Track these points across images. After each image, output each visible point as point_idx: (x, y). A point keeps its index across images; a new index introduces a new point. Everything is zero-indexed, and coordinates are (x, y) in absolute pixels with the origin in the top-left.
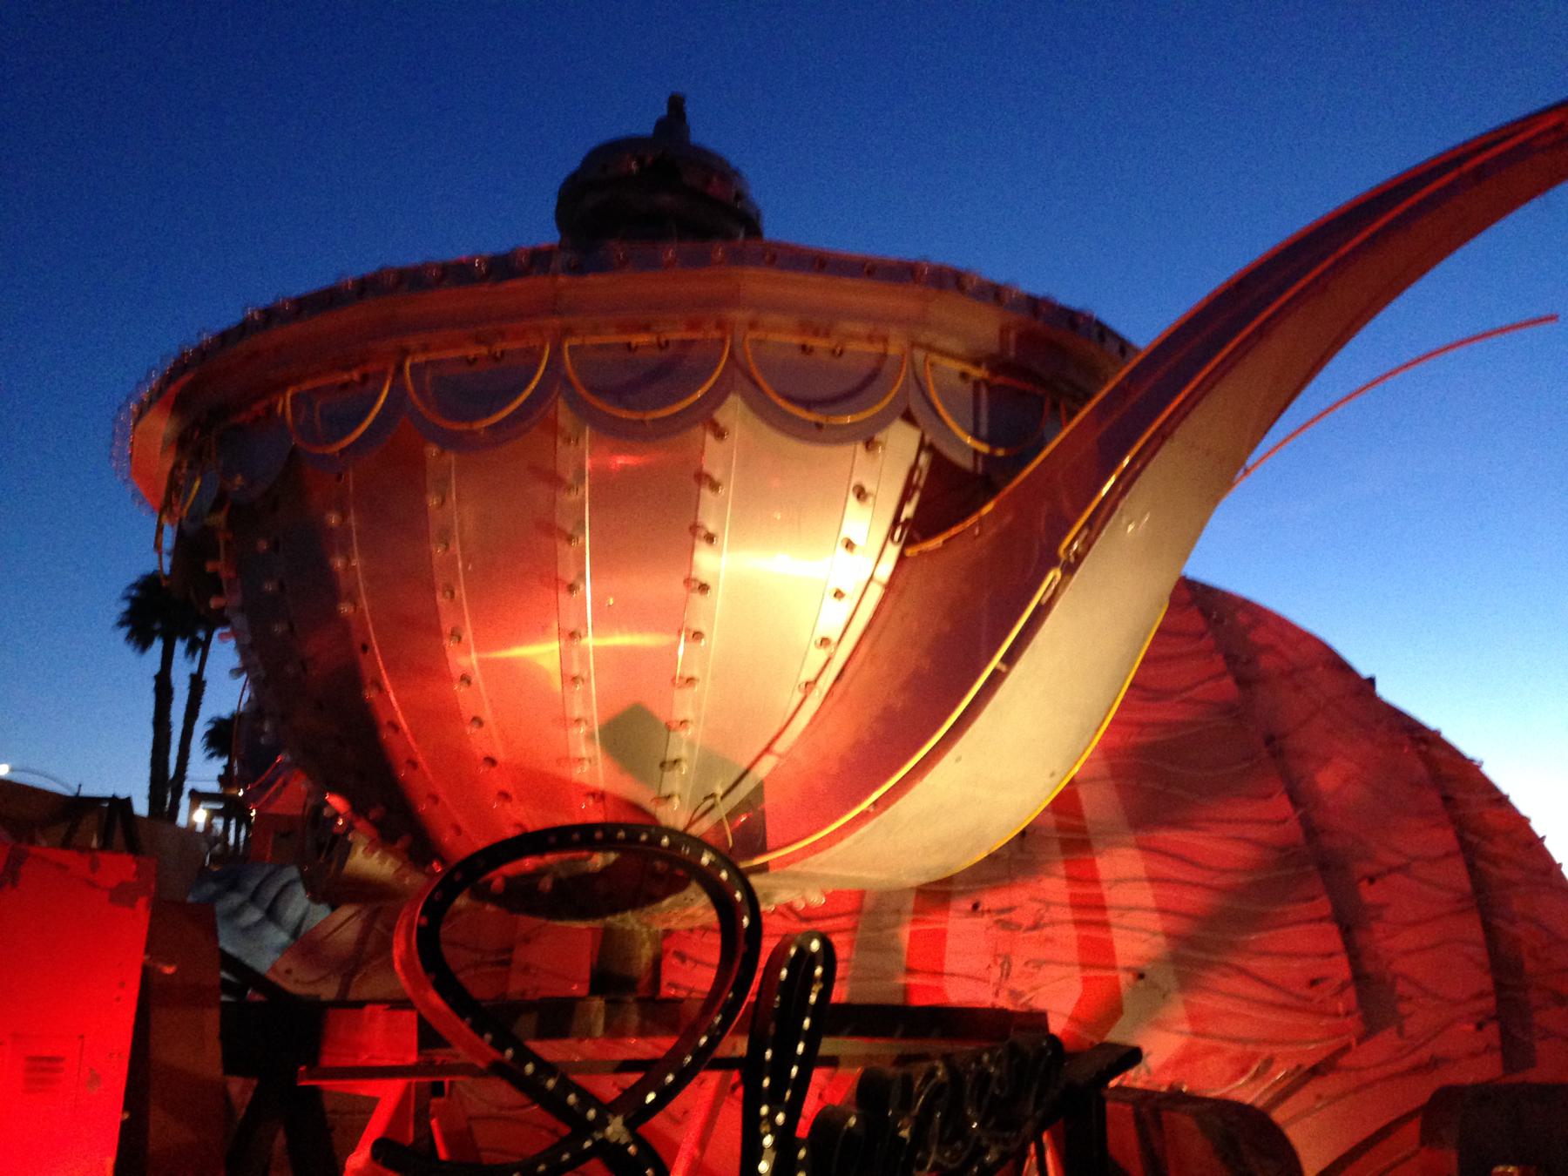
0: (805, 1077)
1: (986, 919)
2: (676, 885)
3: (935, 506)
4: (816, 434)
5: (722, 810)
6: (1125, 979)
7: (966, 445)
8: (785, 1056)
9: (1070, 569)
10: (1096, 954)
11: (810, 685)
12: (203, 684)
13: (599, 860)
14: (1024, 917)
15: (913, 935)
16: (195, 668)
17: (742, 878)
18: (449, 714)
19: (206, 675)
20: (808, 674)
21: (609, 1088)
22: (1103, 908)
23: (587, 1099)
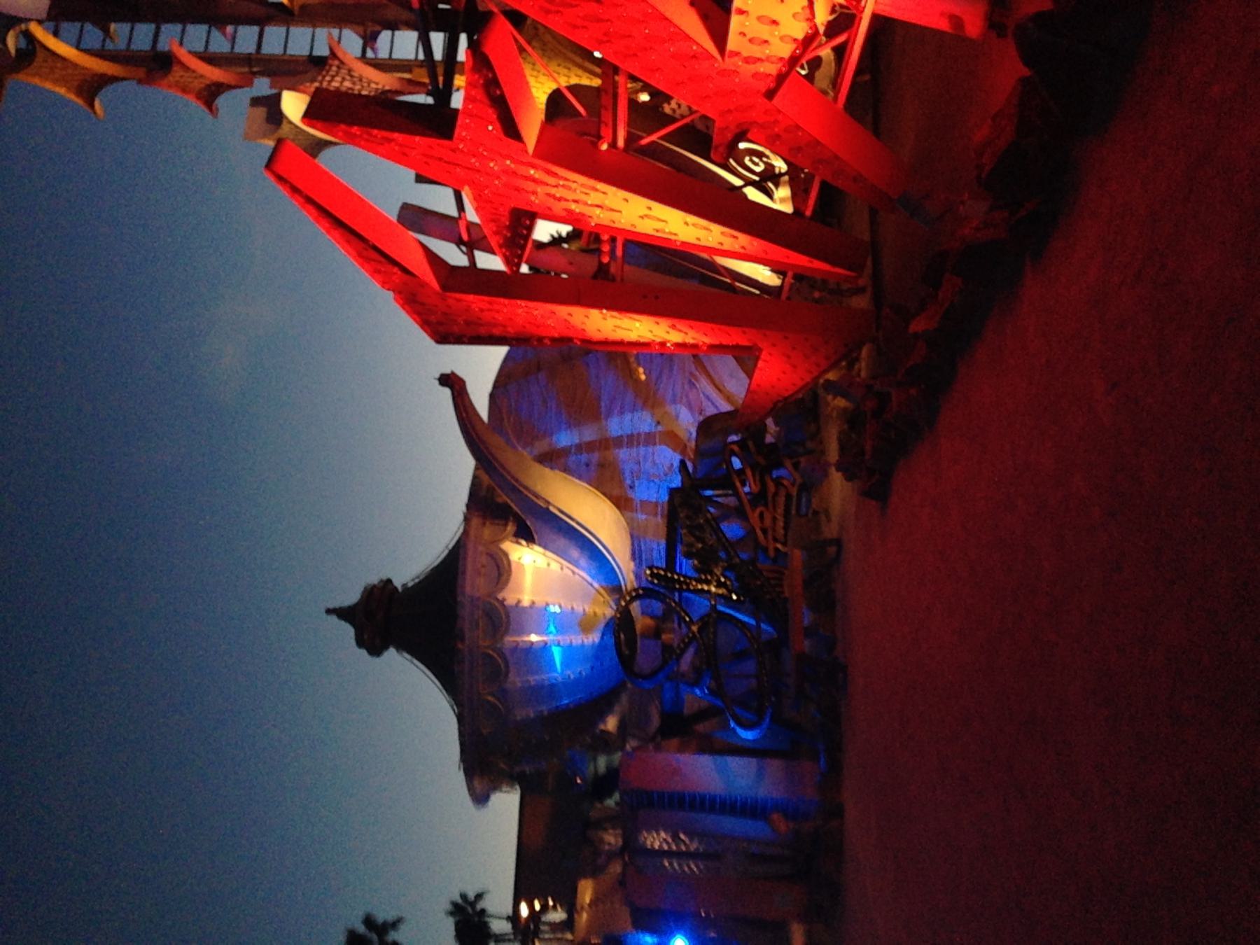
0: (684, 576)
1: (637, 483)
2: (629, 612)
3: (526, 535)
5: (608, 598)
6: (660, 428)
7: (511, 528)
8: (678, 581)
9: (548, 503)
10: (650, 439)
11: (574, 573)
14: (636, 468)
15: (642, 512)
17: (629, 593)
18: (577, 682)
20: (570, 573)
21: (684, 630)
22: (632, 435)
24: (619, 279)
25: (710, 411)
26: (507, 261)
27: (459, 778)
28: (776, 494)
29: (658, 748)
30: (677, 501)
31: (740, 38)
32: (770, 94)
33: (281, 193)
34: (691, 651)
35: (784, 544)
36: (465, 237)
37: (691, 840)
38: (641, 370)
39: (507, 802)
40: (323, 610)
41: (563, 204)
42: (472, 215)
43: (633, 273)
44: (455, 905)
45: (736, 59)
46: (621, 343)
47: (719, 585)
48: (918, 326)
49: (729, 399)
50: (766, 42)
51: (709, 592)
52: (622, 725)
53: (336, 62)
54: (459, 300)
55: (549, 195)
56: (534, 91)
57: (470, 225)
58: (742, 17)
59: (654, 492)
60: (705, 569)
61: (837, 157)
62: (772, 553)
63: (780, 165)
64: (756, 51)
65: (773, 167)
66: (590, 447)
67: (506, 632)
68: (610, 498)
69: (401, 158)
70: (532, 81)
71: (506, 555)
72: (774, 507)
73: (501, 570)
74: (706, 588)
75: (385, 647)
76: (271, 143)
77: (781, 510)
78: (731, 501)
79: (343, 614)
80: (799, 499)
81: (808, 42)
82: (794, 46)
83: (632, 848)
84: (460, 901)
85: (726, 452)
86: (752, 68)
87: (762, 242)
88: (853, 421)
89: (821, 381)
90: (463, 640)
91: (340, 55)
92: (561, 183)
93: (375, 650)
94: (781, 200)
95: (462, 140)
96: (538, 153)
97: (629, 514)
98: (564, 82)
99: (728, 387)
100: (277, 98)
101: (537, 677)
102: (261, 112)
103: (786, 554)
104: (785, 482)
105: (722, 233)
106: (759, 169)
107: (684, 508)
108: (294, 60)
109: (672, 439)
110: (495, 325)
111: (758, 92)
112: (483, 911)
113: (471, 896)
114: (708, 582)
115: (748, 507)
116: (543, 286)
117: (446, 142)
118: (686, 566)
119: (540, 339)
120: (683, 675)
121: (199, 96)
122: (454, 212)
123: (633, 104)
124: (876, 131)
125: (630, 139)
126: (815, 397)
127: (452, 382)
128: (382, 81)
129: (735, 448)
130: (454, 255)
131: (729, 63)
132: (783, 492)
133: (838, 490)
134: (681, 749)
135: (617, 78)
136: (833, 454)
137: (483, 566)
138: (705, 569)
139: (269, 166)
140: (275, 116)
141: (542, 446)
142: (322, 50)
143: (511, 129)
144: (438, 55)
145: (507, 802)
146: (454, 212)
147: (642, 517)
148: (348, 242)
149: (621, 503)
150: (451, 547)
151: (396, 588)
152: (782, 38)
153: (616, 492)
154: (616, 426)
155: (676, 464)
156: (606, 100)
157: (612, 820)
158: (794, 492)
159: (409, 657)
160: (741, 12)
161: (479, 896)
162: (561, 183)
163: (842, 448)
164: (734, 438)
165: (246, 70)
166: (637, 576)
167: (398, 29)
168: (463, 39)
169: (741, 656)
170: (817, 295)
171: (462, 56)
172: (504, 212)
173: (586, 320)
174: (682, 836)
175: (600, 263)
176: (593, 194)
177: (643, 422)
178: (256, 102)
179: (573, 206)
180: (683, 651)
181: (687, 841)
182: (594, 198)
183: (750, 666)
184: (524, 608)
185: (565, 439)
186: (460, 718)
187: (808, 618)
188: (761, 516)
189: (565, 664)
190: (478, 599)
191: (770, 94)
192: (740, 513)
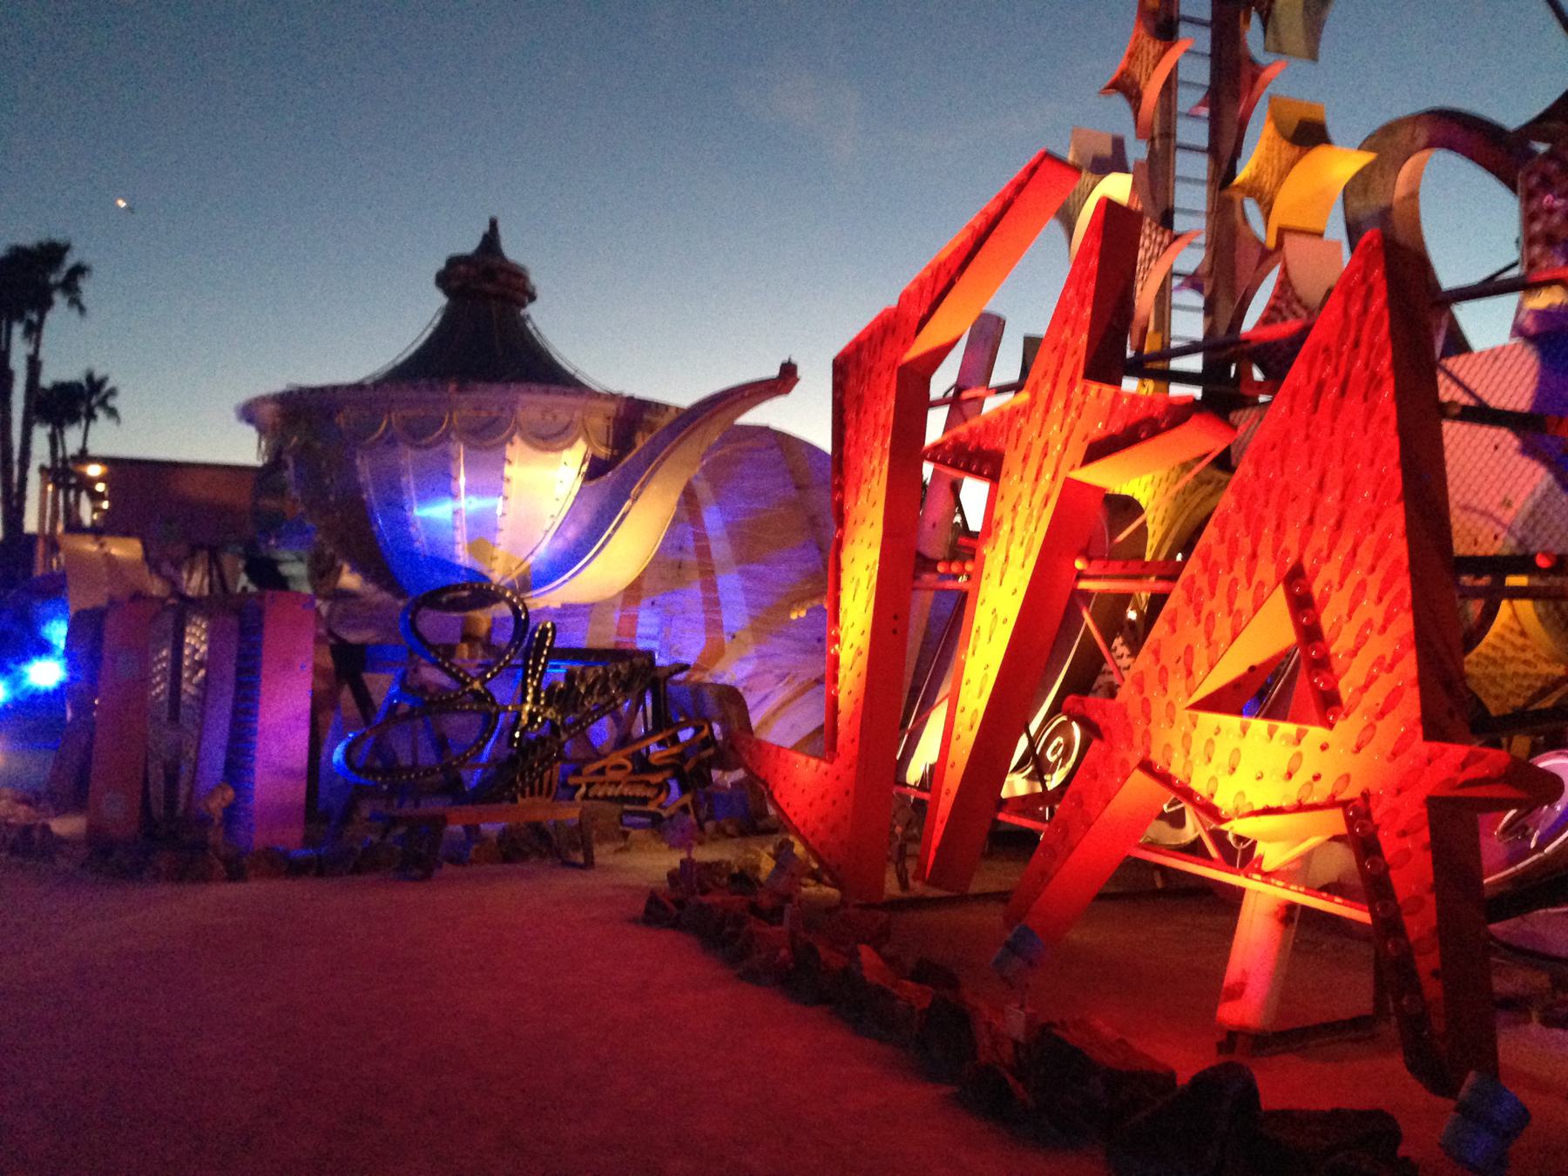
3: (595, 469)
4: (547, 450)
5: (515, 574)
7: (603, 452)
8: (537, 662)
9: (635, 500)
10: (713, 625)
12: (39, 364)
13: (466, 593)
16: (31, 350)
17: (521, 600)
19: (43, 354)
20: (547, 527)
23: (467, 675)
24: (916, 584)
25: (750, 701)
26: (937, 447)
27: (277, 385)
28: (648, 784)
29: (318, 640)
30: (637, 661)
31: (1213, 729)
32: (1147, 766)
33: (1017, 170)
34: (445, 680)
35: (585, 797)
36: (966, 395)
37: (197, 686)
38: (803, 614)
39: (243, 448)
40: (494, 214)
41: (1008, 515)
42: (992, 404)
43: (922, 604)
44: (102, 382)
45: (1189, 723)
46: (837, 587)
47: (532, 717)
48: (866, 954)
49: (765, 723)
50: (1210, 760)
51: (524, 701)
52: (347, 595)
53: (1166, 241)
54: (888, 387)
55: (1020, 496)
56: (1137, 481)
57: (979, 401)
58: (1238, 730)
59: (647, 632)
60: (555, 697)
61: (1072, 849)
62: (572, 781)
63: (1054, 780)
64: (1198, 746)
65: (1052, 772)
66: (704, 552)
67: (469, 446)
68: (640, 578)
69: (1061, 317)
70: (1147, 478)
71: (570, 445)
72: (632, 783)
73: (549, 439)
74: (529, 698)
75: (447, 292)
76: (1070, 157)
77: (627, 791)
78: (639, 729)
79: (491, 241)
80: (642, 814)
81: (1209, 810)
82: (1205, 794)
83: (185, 607)
84: (108, 386)
85: (700, 720)
86: (1177, 744)
87: (966, 758)
88: (744, 879)
89: (791, 838)
90: (460, 390)
91: (1176, 245)
92: (1035, 513)
93: (443, 280)
94: (1017, 785)
95: (1085, 392)
96: (1069, 482)
97: (619, 601)
98: (1149, 516)
99: (780, 721)
100: (1124, 169)
101: (412, 485)
102: (1107, 150)
103: (572, 798)
104: (663, 796)
105: (976, 711)
106: (1051, 758)
107: (632, 671)
108: (1168, 190)
109: (715, 653)
110: (857, 432)
111: (1148, 751)
112: (91, 416)
113: (111, 402)
114: (536, 701)
115: (630, 750)
116: (906, 498)
117: (1081, 373)
118: (558, 673)
119: (840, 488)
120: (416, 671)
121: (1125, 73)
122: (996, 380)
123: (1124, 599)
124: (1101, 897)
125: (1086, 595)
126: (770, 831)
127: (787, 377)
128: (1144, 299)
129: (706, 732)
130: (942, 381)
131: (1182, 715)
132: (649, 793)
133: (654, 863)
134: (318, 671)
135: (1153, 579)
136: (703, 854)
137: (555, 417)
138: (555, 697)
139: (1047, 156)
140: (1102, 167)
141: (704, 490)
142: (1180, 223)
143: (1097, 451)
144: (1177, 364)
145: (243, 448)
146: (996, 380)
147: (615, 617)
148: (956, 252)
149: (634, 591)
150: (578, 376)
151: (523, 306)
152: (1213, 779)
153: (646, 585)
154: (729, 582)
155: (684, 659)
156: (1133, 567)
157: (220, 582)
158: (652, 807)
159: (436, 322)
160: (1244, 730)
161: (112, 412)
162: (1035, 513)
163: (707, 866)
164: (717, 728)
165: (1156, 131)
166: (541, 612)
167: (1206, 315)
168: (1197, 392)
169: (441, 745)
170: (898, 829)
171: (1177, 390)
172: (999, 443)
173: (866, 544)
174: (202, 673)
175: (936, 562)
176: (1022, 551)
177: (735, 616)
178: (1118, 144)
179: (1006, 527)
180: (447, 671)
181: (195, 680)
182: (1017, 553)
183: (427, 757)
184: (501, 469)
185: (712, 519)
186: (359, 387)
187: (490, 829)
188: (620, 767)
189: (427, 522)
190: (513, 411)
191: (1147, 766)
192: (624, 741)
